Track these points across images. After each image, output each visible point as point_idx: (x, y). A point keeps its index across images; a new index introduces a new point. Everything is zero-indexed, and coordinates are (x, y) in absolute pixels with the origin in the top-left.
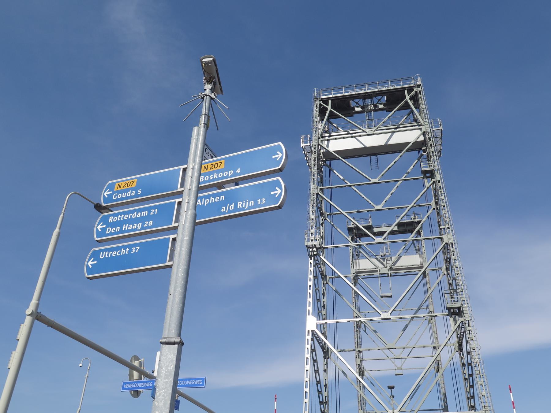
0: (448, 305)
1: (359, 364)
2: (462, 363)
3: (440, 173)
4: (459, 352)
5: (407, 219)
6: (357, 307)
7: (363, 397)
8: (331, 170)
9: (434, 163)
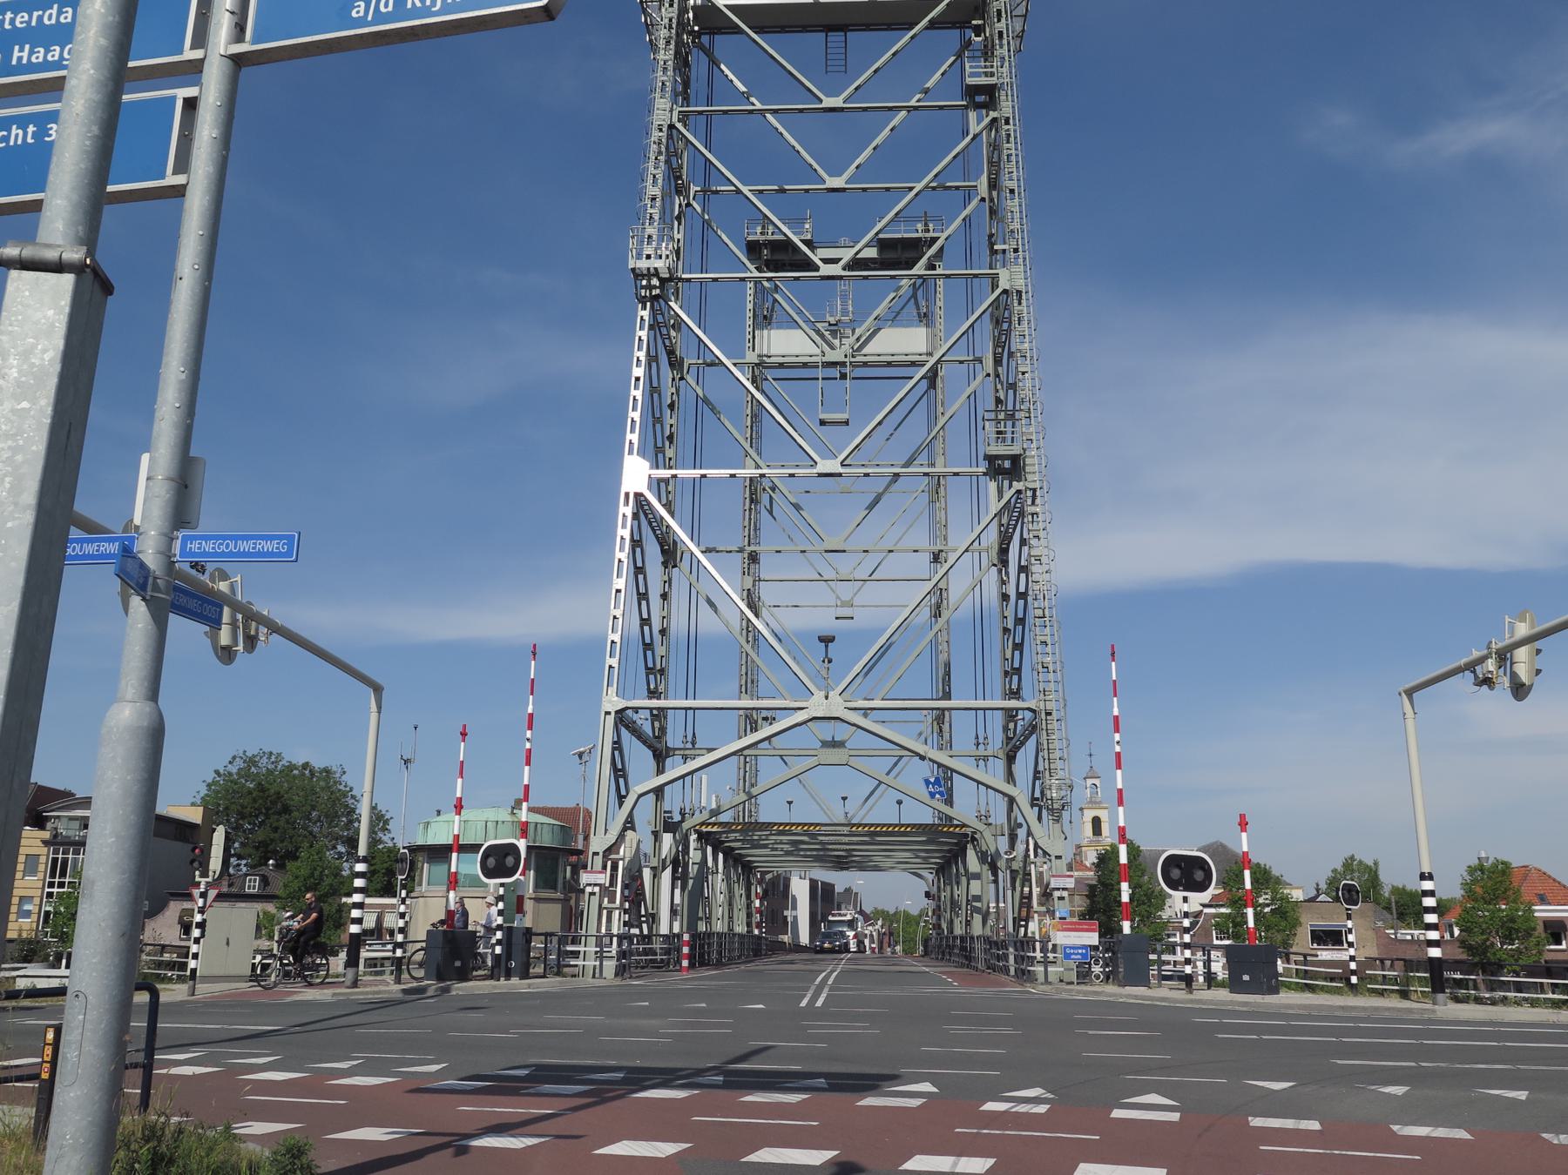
0: (989, 448)
1: (749, 590)
2: (1003, 594)
3: (1012, 96)
4: (1000, 566)
5: (905, 232)
6: (756, 439)
7: (753, 661)
8: (714, 63)
9: (1002, 67)
